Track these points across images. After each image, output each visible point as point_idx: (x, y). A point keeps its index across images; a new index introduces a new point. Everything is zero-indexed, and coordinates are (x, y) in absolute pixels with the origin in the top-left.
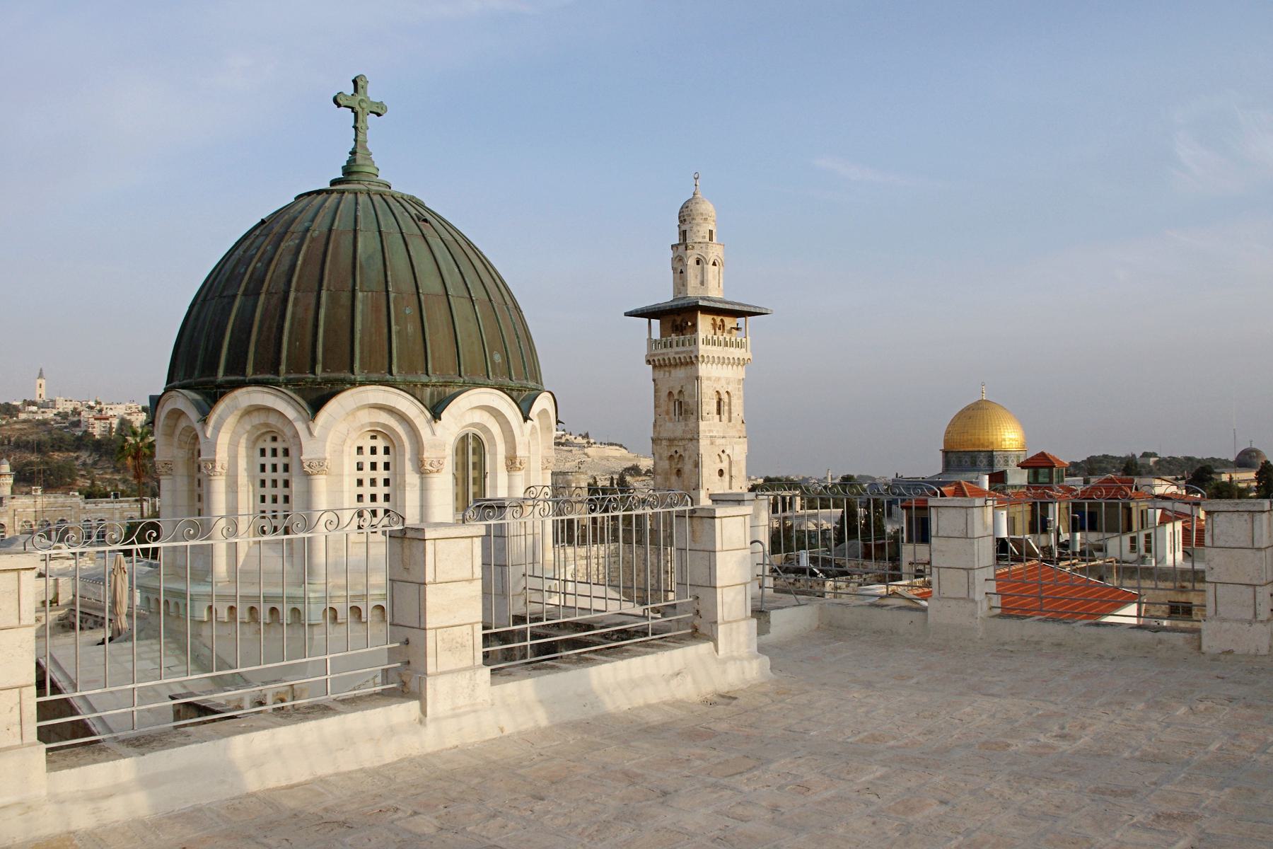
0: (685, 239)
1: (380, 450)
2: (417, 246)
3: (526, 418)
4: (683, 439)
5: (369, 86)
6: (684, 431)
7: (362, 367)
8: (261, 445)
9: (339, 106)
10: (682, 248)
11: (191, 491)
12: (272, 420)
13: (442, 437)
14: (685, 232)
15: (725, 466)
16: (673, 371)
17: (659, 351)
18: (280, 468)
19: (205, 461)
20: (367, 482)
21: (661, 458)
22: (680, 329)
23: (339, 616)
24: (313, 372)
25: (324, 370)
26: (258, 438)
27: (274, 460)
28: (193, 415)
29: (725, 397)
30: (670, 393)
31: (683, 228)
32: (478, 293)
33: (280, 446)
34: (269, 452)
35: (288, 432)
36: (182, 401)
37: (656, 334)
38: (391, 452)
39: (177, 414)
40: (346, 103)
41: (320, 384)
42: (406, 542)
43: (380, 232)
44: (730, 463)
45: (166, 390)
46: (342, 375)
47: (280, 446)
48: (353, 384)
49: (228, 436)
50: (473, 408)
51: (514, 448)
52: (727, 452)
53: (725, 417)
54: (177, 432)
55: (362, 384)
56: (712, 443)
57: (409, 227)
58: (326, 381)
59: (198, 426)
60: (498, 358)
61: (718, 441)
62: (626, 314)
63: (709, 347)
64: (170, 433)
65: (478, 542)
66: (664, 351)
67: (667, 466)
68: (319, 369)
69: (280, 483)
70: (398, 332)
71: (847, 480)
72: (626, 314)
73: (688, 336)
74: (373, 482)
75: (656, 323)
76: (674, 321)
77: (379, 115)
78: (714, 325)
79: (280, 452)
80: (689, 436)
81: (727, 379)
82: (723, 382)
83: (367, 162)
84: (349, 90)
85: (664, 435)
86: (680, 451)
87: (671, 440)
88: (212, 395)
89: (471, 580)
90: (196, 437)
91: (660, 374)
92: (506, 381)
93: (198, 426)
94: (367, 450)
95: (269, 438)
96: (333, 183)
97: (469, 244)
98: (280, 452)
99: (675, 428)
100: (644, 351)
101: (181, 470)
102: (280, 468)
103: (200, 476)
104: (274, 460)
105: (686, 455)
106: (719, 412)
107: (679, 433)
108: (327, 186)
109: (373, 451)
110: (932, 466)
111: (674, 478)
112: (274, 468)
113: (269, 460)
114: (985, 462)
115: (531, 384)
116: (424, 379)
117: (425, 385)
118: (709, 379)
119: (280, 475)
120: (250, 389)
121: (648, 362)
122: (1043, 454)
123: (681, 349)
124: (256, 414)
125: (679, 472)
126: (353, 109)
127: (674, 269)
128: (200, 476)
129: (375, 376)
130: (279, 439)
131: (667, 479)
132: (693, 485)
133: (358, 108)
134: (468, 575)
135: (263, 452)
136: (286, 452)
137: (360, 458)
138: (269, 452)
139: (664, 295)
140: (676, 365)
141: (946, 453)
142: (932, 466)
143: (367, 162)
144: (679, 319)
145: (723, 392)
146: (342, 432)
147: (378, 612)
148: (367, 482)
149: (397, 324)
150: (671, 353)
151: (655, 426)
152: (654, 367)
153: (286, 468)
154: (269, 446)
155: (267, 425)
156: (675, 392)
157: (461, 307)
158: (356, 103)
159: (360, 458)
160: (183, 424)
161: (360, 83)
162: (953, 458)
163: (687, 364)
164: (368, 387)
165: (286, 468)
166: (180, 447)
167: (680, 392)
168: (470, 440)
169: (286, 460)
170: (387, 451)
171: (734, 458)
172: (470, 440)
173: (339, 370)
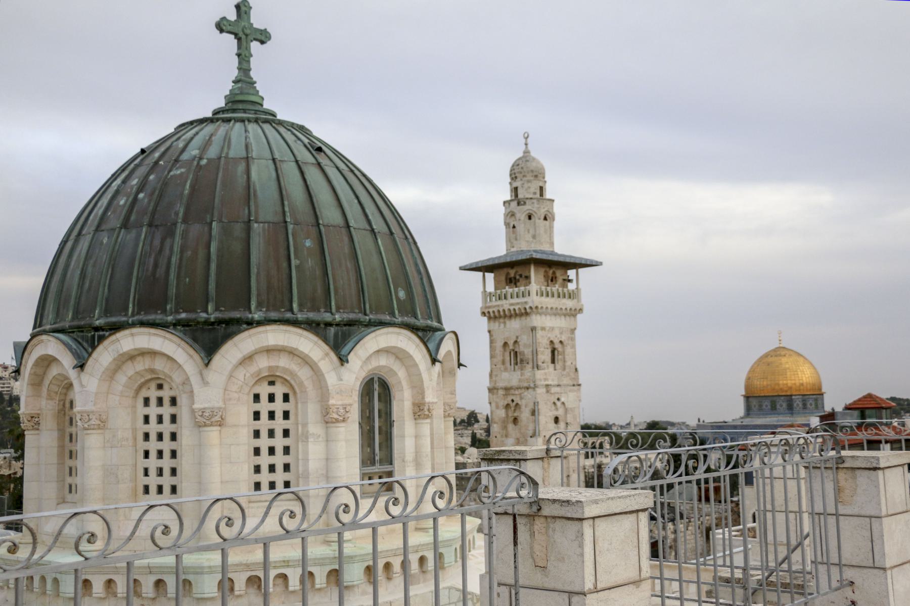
0: (516, 196)
1: (279, 398)
2: (313, 175)
3: (434, 361)
4: (518, 388)
5: (252, 12)
6: (520, 380)
7: (260, 305)
8: (144, 393)
9: (222, 31)
10: (514, 204)
11: (61, 447)
12: (159, 364)
13: (345, 381)
14: (516, 189)
15: (560, 413)
16: (508, 322)
17: (494, 303)
18: (167, 419)
19: (80, 412)
20: (264, 434)
21: (497, 407)
22: (512, 281)
23: (236, 588)
24: (206, 311)
25: (217, 309)
26: (140, 387)
27: (160, 411)
28: (67, 360)
29: (558, 346)
30: (505, 344)
31: (515, 185)
32: (378, 224)
33: (166, 394)
34: (153, 402)
35: (177, 378)
36: (51, 346)
37: (490, 288)
38: (276, 401)
39: (48, 361)
40: (229, 28)
41: (213, 324)
42: (539, 524)
43: (274, 160)
44: (566, 410)
45: (33, 336)
46: (236, 315)
47: (166, 394)
48: (251, 324)
49: (103, 385)
50: (382, 347)
51: (422, 393)
52: (563, 399)
53: (559, 365)
54: (46, 382)
55: (259, 323)
56: (548, 392)
57: (305, 156)
58: (220, 322)
59: (73, 374)
60: (402, 294)
61: (553, 390)
62: (462, 268)
63: (544, 299)
64: (37, 383)
65: (644, 518)
66: (499, 303)
67: (504, 415)
68: (210, 308)
69: (167, 437)
70: (297, 267)
71: (653, 425)
72: (462, 268)
73: (522, 288)
74: (271, 433)
75: (490, 276)
76: (508, 274)
77: (262, 42)
78: (546, 276)
79: (166, 401)
80: (526, 385)
81: (560, 328)
82: (557, 332)
83: (251, 91)
84: (232, 16)
85: (501, 384)
86: (517, 400)
87: (507, 389)
88: (87, 338)
89: (636, 583)
90: (70, 386)
91: (495, 326)
92: (412, 320)
93: (73, 374)
94: (264, 398)
95: (153, 385)
96: (216, 112)
97: (364, 175)
98: (166, 401)
99: (511, 377)
100: (478, 303)
101: (49, 424)
102: (167, 419)
103: (73, 430)
104: (160, 411)
105: (523, 403)
106: (553, 361)
107: (515, 383)
108: (209, 115)
109: (271, 398)
110: (732, 409)
111: (511, 426)
112: (160, 419)
113: (153, 411)
114: (785, 405)
115: (435, 324)
116: (328, 317)
117: (328, 324)
118: (543, 329)
119: (167, 428)
120: (135, 330)
121: (484, 314)
122: (870, 396)
123: (515, 300)
124: (139, 359)
125: (515, 420)
126: (236, 35)
127: (507, 224)
128: (73, 430)
129: (273, 315)
130: (166, 387)
131: (505, 428)
132: (530, 433)
133: (241, 34)
134: (633, 575)
135: (147, 402)
136: (173, 401)
137: (257, 407)
138: (153, 402)
139: (498, 250)
140: (511, 316)
141: (747, 398)
142: (732, 409)
143: (251, 91)
144: (512, 272)
145: (556, 341)
146: (222, 383)
147: (280, 581)
148: (264, 434)
149: (296, 257)
150: (506, 305)
151: (491, 375)
152: (490, 318)
153: (174, 419)
154: (153, 394)
155: (152, 371)
156: (511, 343)
157: (362, 239)
158: (242, 31)
159: (257, 407)
160: (54, 371)
161: (243, 9)
162: (754, 402)
163: (521, 315)
164: (268, 328)
165: (174, 419)
166: (50, 397)
167: (516, 342)
168: (376, 386)
169: (173, 410)
170: (286, 398)
171: (568, 405)
172: (376, 386)
173: (235, 308)
